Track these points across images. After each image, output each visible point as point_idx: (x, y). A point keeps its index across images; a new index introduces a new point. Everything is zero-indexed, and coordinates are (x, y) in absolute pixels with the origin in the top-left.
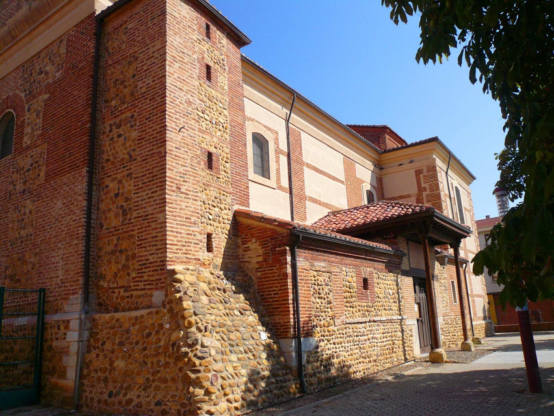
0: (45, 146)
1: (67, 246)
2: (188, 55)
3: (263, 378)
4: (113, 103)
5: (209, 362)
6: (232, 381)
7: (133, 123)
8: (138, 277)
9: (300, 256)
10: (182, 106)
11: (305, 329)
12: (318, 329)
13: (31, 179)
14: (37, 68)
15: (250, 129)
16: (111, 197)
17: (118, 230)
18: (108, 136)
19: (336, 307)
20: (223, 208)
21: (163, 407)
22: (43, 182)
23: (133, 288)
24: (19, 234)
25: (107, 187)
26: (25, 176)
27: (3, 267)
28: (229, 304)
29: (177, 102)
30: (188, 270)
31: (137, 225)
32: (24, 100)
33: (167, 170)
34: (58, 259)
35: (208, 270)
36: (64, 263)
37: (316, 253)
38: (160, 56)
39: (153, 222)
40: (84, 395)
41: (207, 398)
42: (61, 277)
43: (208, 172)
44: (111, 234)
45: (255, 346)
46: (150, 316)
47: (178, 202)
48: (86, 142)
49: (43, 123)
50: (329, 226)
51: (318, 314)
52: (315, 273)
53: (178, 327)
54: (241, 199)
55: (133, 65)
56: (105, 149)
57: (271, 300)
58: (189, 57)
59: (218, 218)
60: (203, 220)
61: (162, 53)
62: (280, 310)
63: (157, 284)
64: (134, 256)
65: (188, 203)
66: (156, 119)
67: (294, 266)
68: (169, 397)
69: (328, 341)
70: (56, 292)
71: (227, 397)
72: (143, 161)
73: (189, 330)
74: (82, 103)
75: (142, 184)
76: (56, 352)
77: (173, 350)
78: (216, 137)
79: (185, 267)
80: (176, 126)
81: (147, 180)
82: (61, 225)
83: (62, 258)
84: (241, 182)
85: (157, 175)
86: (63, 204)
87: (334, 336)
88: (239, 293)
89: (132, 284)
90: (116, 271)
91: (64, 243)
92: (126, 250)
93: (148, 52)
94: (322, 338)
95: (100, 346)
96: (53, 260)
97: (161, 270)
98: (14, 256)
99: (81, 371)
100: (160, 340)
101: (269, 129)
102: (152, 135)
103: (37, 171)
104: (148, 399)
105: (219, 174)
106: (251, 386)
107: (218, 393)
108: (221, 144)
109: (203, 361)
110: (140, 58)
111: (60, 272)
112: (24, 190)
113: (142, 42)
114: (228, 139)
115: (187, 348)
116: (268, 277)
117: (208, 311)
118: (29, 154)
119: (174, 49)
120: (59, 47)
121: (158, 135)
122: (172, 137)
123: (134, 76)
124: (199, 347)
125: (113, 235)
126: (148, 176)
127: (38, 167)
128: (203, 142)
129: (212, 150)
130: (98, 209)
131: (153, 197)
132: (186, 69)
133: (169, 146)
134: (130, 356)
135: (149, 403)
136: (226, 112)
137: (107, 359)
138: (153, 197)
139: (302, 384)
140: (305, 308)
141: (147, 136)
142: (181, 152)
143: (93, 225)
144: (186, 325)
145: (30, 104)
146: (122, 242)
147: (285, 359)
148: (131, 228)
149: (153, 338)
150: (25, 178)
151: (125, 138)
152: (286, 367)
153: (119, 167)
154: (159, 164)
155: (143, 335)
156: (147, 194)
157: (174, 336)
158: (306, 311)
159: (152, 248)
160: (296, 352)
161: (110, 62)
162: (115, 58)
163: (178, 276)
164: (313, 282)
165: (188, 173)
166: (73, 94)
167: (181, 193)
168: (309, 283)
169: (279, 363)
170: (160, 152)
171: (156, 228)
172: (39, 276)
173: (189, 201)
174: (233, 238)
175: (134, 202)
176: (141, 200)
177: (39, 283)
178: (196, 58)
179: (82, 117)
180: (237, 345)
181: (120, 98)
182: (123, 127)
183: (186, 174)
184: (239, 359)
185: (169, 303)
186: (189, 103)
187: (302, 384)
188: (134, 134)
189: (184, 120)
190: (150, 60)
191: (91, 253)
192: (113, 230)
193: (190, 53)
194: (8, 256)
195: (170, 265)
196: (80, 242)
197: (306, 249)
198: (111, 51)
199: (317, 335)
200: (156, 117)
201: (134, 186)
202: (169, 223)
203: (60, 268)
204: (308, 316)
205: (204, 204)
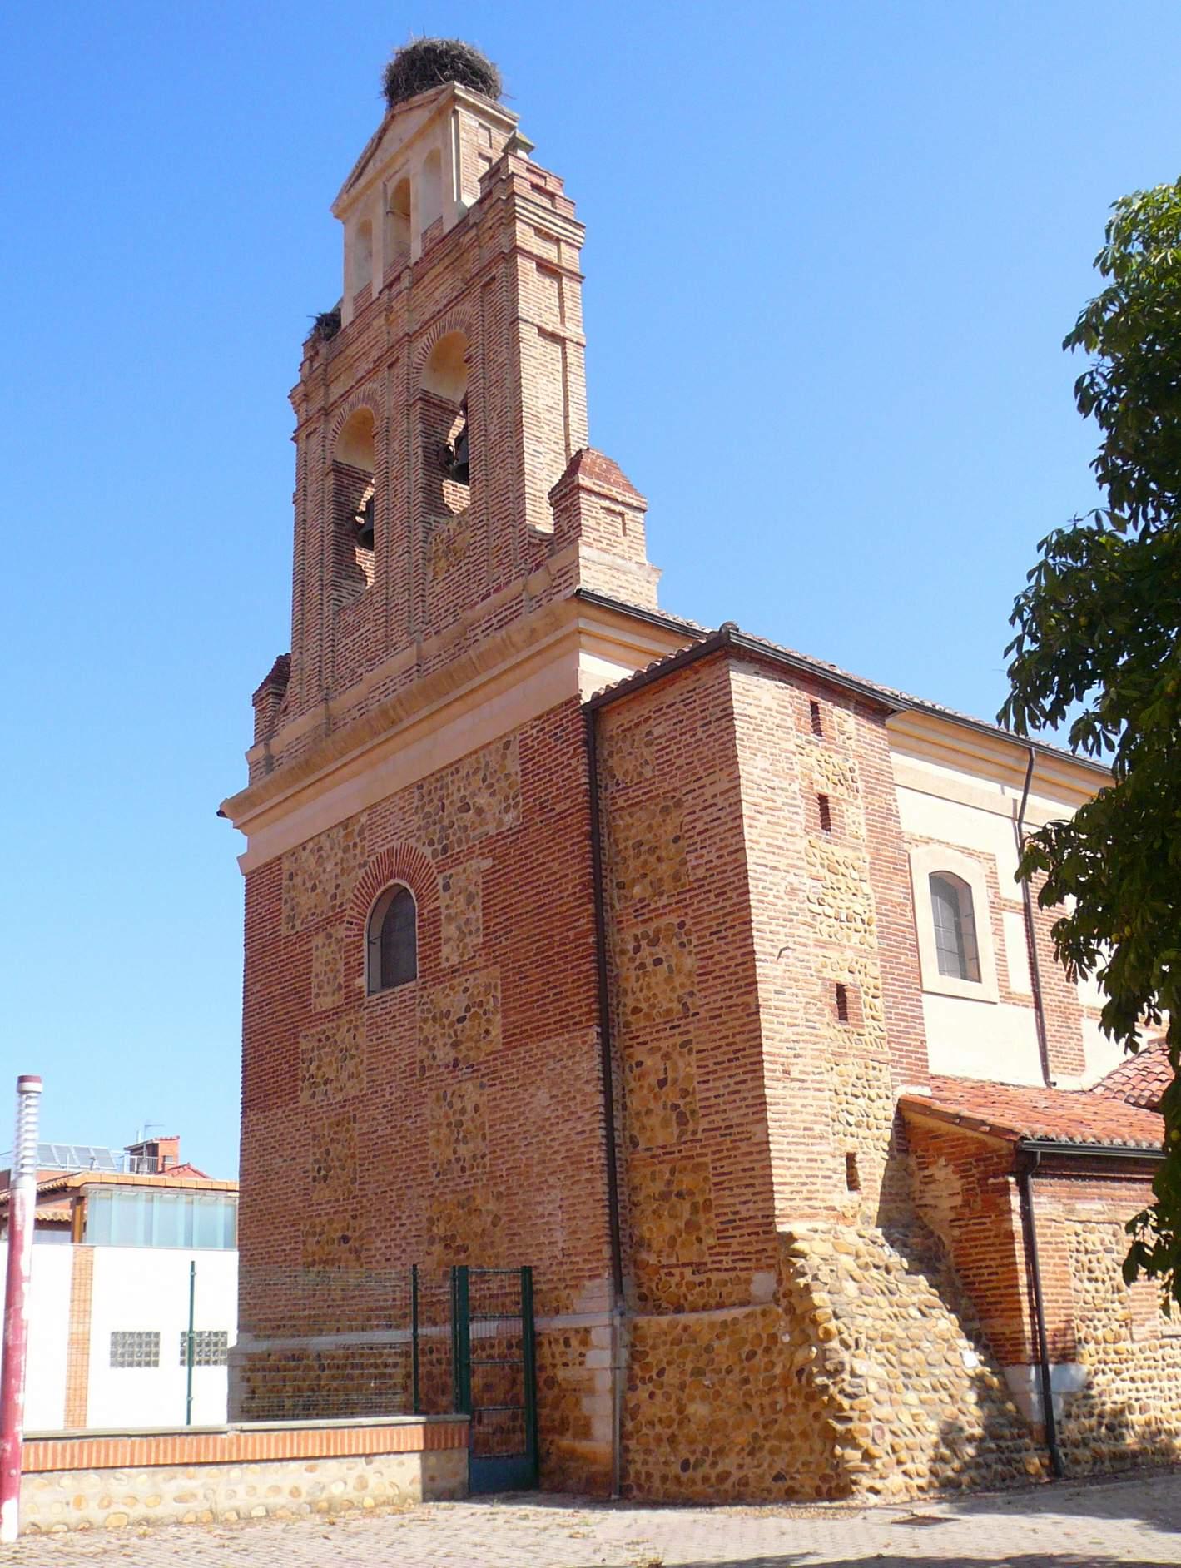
0: (496, 971)
1: (568, 1183)
2: (782, 790)
3: (971, 1439)
4: (637, 890)
5: (866, 1403)
6: (910, 1440)
7: (685, 939)
8: (720, 1245)
9: (1040, 1194)
10: (780, 903)
11: (1059, 1346)
12: (1091, 1347)
13: (470, 1038)
14: (456, 797)
15: (924, 865)
16: (649, 1085)
17: (672, 1153)
18: (632, 960)
19: (1133, 1300)
20: (874, 1097)
21: (789, 1483)
22: (500, 1047)
23: (710, 1266)
24: (455, 1152)
25: (639, 1064)
26: (455, 1031)
27: (424, 1220)
28: (897, 1297)
29: (771, 898)
30: (816, 1231)
31: (709, 1145)
32: (433, 862)
33: (764, 1041)
34: (551, 1207)
35: (853, 1229)
36: (567, 1216)
37: (1080, 1183)
38: (730, 805)
39: (741, 1140)
40: (632, 1470)
41: (866, 1465)
42: (561, 1245)
43: (840, 1027)
44: (656, 1160)
45: (953, 1379)
46: (751, 1320)
47: (789, 1100)
48: (592, 975)
49: (485, 922)
50: (1144, 1084)
51: (1090, 1315)
52: (1079, 1227)
53: (806, 1341)
54: (911, 1070)
55: (674, 814)
56: (625, 985)
57: (983, 1286)
58: (784, 794)
59: (865, 1119)
60: (838, 1127)
61: (732, 801)
62: (1003, 1306)
63: (758, 1260)
64: (708, 1206)
65: (806, 1098)
66: (734, 935)
67: (1027, 1216)
68: (798, 1465)
69: (1117, 1373)
70: (553, 1273)
71: (903, 1468)
72: (712, 1018)
73: (827, 1346)
74: (571, 891)
75: (715, 1064)
76: (567, 1390)
77: (800, 1380)
78: (851, 948)
79: (810, 1227)
80: (773, 946)
81: (725, 1058)
82: (551, 1140)
83: (560, 1207)
84: (909, 1033)
85: (744, 1050)
86: (552, 1097)
87: (1131, 1364)
88: (916, 1273)
89: (708, 1259)
90: (673, 1233)
91: (562, 1176)
92: (691, 1194)
93: (703, 794)
94: (1102, 1366)
95: (655, 1377)
96: (540, 1209)
97: (765, 1233)
98: (448, 1197)
99: (622, 1425)
100: (773, 1364)
101: (971, 853)
102: (727, 967)
103: (483, 1021)
104: (759, 1471)
105: (862, 1027)
106: (944, 1451)
107: (885, 1458)
108: (861, 960)
109: (856, 1402)
110: (686, 805)
111: (558, 1234)
112: (456, 1063)
113: (688, 771)
114: (876, 946)
115: (825, 1378)
116: (975, 1239)
117: (860, 1311)
118: (460, 984)
119: (755, 786)
120: (504, 757)
121: (740, 969)
122: (766, 972)
123: (676, 840)
124: (846, 1376)
125: (661, 1162)
126: (725, 1049)
127: (485, 1014)
128: (824, 966)
129: (845, 978)
130: (624, 1107)
131: (738, 1092)
132: (782, 821)
133: (764, 991)
134: (717, 1394)
135: (761, 1478)
136: (866, 888)
137: (672, 1402)
138: (738, 1092)
139: (1054, 1458)
140: (1057, 1301)
141: (717, 968)
142: (786, 997)
143: (617, 1141)
144: (821, 1336)
145: (448, 873)
146: (681, 1176)
147: (1017, 1407)
148: (699, 1151)
149: (760, 1360)
150: (456, 1035)
151: (670, 966)
152: (1019, 1422)
153: (662, 1026)
154: (747, 1028)
155: (740, 1355)
156: (728, 1086)
157: (799, 1357)
158: (1060, 1308)
159: (744, 1191)
160: (1039, 1393)
161: (621, 803)
162: (631, 795)
163: (798, 1245)
164: (1075, 1246)
165: (801, 1038)
166: (550, 868)
167: (793, 1080)
168: (1064, 1250)
169: (1003, 1413)
170: (747, 1005)
171: (751, 1153)
172: (511, 1241)
173: (807, 1093)
174: (899, 1157)
175: (700, 1100)
176: (716, 1097)
177: (513, 1254)
178: (797, 790)
179: (576, 921)
180: (918, 1375)
181: (651, 883)
182: (663, 943)
183: (797, 1041)
184: (922, 1402)
185: (785, 1296)
186: (793, 892)
187: (1054, 1458)
188: (690, 962)
189: (786, 930)
190: (709, 810)
191: (620, 1198)
192: (660, 1151)
193: (785, 785)
194: (432, 1196)
195: (782, 1223)
196: (597, 1176)
197: (1053, 1176)
198: (619, 776)
199: (1089, 1360)
200: (733, 931)
201: (698, 1067)
202: (775, 1143)
203: (558, 1227)
204: (1064, 1318)
205: (837, 1094)
